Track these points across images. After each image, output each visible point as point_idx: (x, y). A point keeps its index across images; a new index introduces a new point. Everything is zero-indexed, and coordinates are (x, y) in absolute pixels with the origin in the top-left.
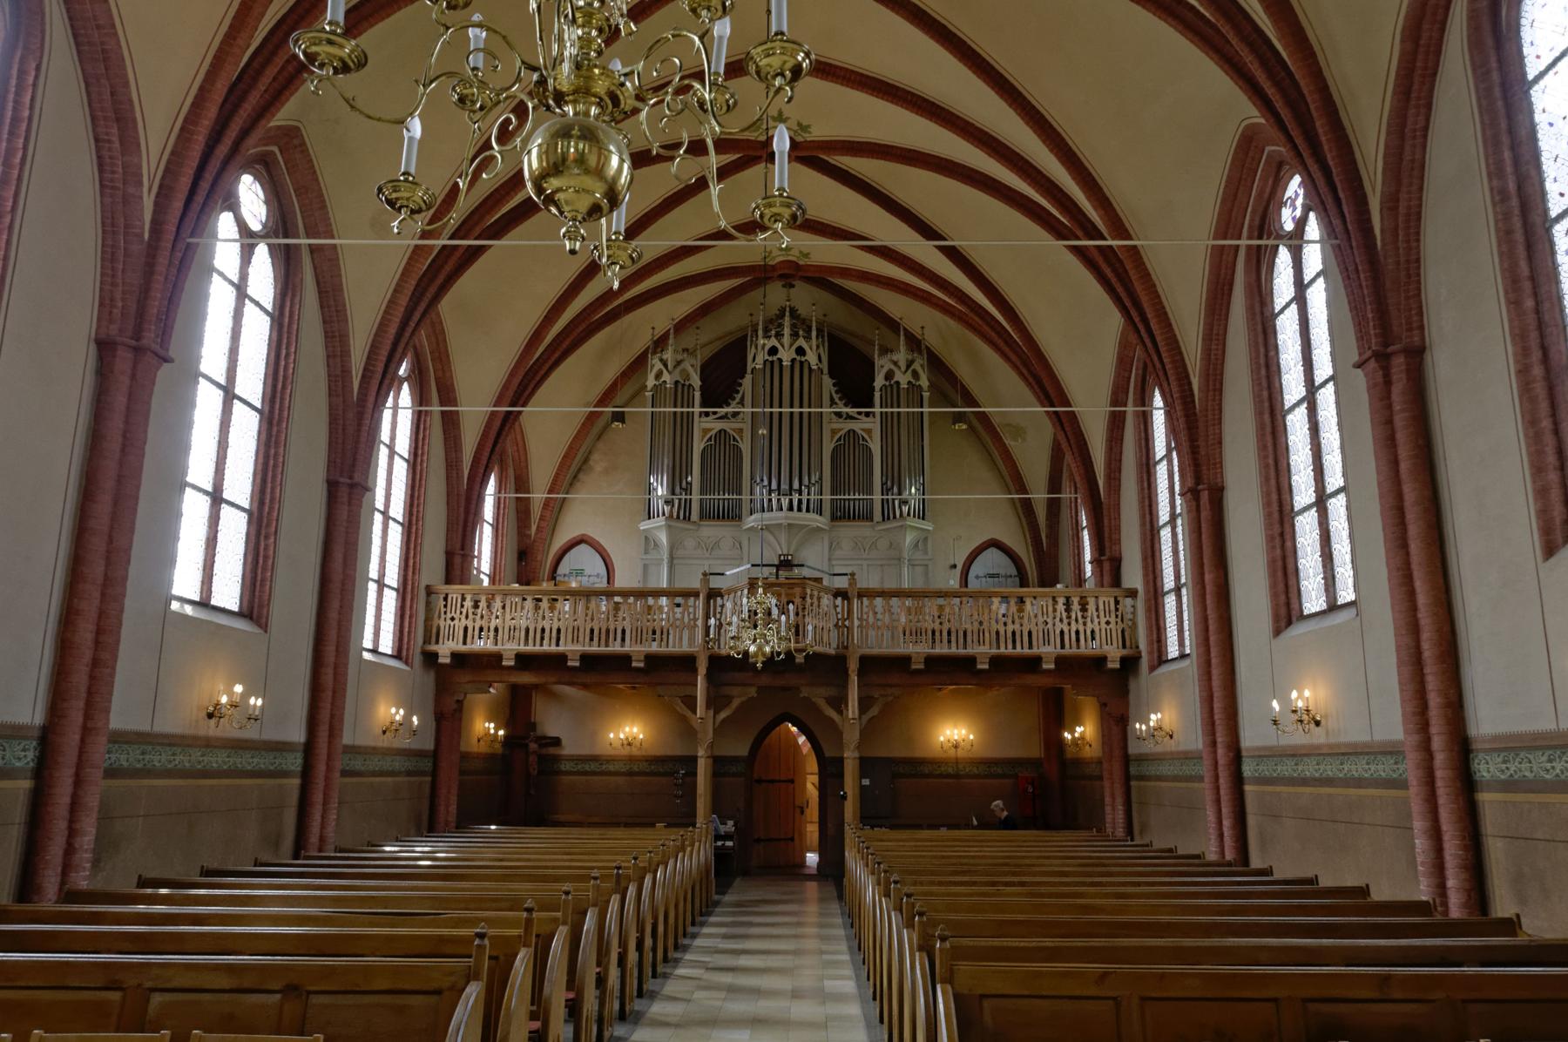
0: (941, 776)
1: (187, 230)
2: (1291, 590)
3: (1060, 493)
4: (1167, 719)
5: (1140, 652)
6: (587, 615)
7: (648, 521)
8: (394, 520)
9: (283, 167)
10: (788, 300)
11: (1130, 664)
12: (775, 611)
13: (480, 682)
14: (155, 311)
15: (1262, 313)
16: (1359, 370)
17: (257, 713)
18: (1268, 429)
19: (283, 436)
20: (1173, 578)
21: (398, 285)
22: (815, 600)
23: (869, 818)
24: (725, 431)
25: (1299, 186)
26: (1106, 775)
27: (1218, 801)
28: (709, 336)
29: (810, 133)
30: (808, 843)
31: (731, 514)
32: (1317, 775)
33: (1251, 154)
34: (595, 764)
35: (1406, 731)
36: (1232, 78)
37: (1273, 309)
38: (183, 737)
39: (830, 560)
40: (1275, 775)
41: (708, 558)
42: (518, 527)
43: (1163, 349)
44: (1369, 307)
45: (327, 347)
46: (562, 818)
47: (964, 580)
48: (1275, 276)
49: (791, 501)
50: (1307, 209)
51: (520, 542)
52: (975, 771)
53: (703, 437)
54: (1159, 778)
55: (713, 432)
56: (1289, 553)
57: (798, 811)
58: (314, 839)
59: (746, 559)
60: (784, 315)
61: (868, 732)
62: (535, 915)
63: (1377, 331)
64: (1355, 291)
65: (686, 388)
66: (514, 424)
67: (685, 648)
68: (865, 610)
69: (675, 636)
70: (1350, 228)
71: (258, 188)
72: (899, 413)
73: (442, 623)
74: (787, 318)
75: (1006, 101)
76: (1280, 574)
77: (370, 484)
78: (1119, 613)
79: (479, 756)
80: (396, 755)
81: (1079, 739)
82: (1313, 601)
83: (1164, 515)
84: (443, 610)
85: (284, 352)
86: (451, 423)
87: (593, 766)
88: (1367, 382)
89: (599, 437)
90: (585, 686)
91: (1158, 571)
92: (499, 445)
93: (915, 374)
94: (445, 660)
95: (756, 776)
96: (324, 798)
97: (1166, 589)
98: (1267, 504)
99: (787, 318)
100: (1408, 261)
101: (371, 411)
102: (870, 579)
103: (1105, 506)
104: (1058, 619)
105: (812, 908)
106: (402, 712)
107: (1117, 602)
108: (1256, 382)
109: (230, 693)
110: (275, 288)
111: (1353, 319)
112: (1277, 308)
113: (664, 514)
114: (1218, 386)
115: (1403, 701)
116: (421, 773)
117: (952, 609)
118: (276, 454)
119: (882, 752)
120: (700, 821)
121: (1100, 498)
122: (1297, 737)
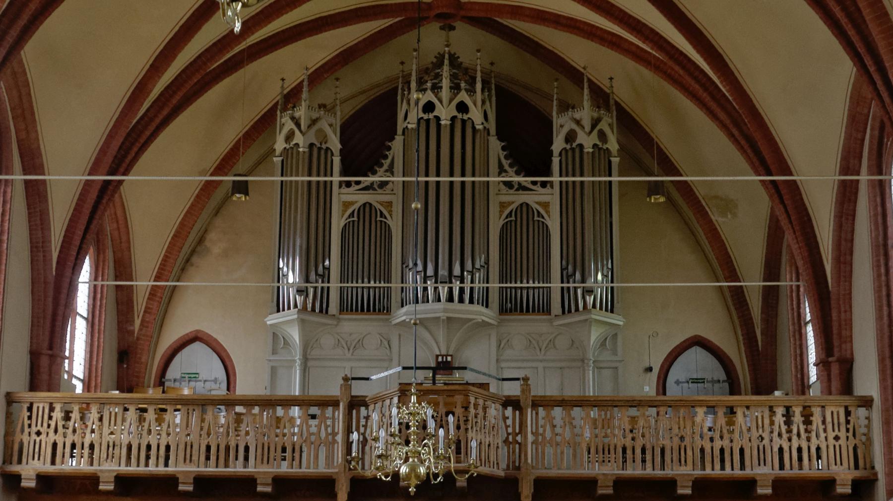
3: (778, 281)
5: (876, 474)
6: (202, 429)
10: (447, 46)
12: (431, 424)
22: (480, 411)
24: (370, 205)
39: (497, 360)
41: (350, 360)
42: (119, 322)
49: (451, 289)
51: (121, 340)
53: (344, 211)
55: (356, 207)
60: (442, 63)
65: (323, 152)
66: (113, 196)
67: (322, 469)
68: (541, 422)
69: (309, 455)
72: (582, 183)
73: (25, 438)
74: (446, 68)
78: (851, 427)
84: (27, 422)
89: (217, 212)
93: (602, 136)
94: (29, 483)
99: (446, 68)
103: (833, 297)
104: (776, 434)
107: (848, 413)
113: (296, 306)
121: (827, 286)
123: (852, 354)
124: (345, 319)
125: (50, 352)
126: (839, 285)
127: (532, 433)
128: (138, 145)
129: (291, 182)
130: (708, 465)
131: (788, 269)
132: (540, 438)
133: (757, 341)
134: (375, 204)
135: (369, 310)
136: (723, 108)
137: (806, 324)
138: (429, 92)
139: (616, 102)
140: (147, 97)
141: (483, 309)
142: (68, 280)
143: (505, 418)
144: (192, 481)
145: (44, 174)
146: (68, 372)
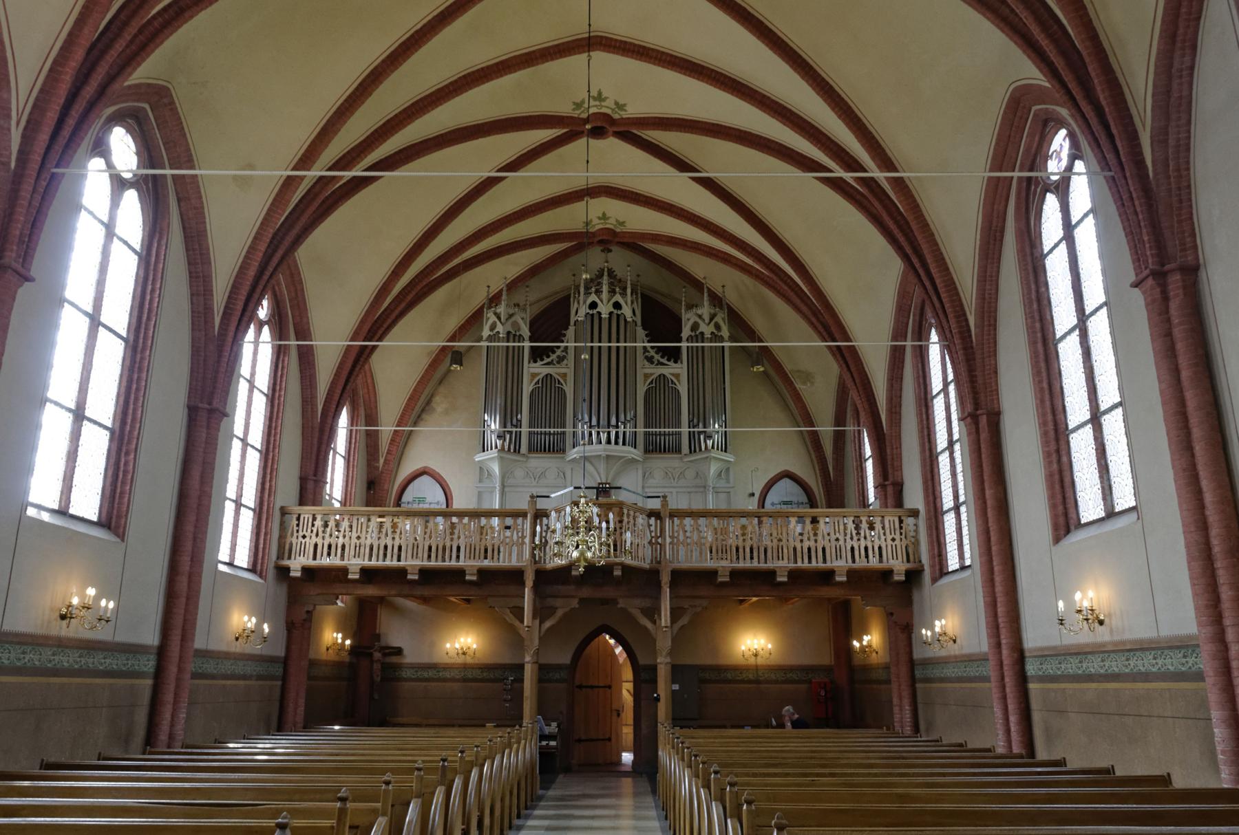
0: (742, 681)
1: (54, 156)
2: (1068, 501)
3: (845, 426)
4: (950, 625)
5: (923, 566)
6: (425, 533)
7: (482, 454)
8: (253, 447)
9: (154, 124)
10: (607, 262)
11: (914, 576)
12: (596, 520)
13: (327, 594)
14: (18, 233)
15: (1032, 254)
16: (1136, 289)
17: (108, 615)
18: (1042, 357)
19: (147, 362)
20: (952, 498)
21: (257, 233)
22: (631, 518)
23: (679, 720)
24: (551, 375)
25: (1064, 139)
26: (893, 678)
27: (1004, 698)
28: (538, 294)
29: (625, 111)
30: (624, 744)
31: (555, 447)
32: (1102, 671)
33: (1019, 114)
34: (435, 672)
35: (1200, 624)
36: (1007, 35)
37: (1042, 250)
38: (32, 636)
40: (1059, 673)
41: (535, 486)
42: (368, 460)
43: (942, 291)
44: (1144, 231)
45: (191, 286)
46: (401, 720)
47: (762, 503)
48: (1043, 221)
49: (609, 433)
50: (1073, 158)
51: (369, 473)
52: (773, 677)
53: (532, 380)
54: (942, 680)
55: (541, 377)
56: (1066, 467)
57: (615, 714)
58: (163, 737)
59: (569, 484)
60: (603, 275)
61: (680, 639)
62: (349, 805)
63: (1153, 252)
64: (1130, 218)
66: (363, 366)
67: (514, 562)
68: (676, 528)
69: (505, 552)
70: (1123, 160)
71: (129, 140)
72: (703, 347)
73: (294, 540)
74: (605, 277)
75: (799, 73)
76: (1057, 487)
77: (228, 410)
78: (903, 531)
79: (326, 663)
80: (247, 660)
81: (867, 647)
82: (1090, 506)
83: (941, 441)
85: (150, 287)
86: (306, 358)
87: (431, 674)
88: (1145, 299)
89: (441, 382)
90: (425, 600)
91: (937, 493)
92: (350, 384)
93: (718, 327)
95: (577, 683)
96: (175, 698)
97: (945, 508)
98: (1043, 424)
99: (605, 277)
100: (1179, 189)
101: (230, 344)
102: (679, 502)
103: (887, 437)
105: (627, 802)
106: (254, 620)
107: (901, 521)
108: (1029, 315)
109: (83, 595)
110: (144, 230)
111: (1128, 243)
112: (1046, 250)
113: (496, 447)
114: (992, 322)
115: (1195, 595)
116: (271, 678)
117: (753, 527)
118: (139, 379)
119: (689, 661)
120: (526, 721)
121: (883, 430)
122: (1082, 636)
123: (902, 479)
124: (532, 457)
125: (315, 478)
126: (891, 430)
127: (670, 537)
128: (383, 329)
129: (494, 346)
130: (799, 560)
131: (852, 421)
132: (675, 540)
133: (829, 475)
134: (554, 374)
135: (549, 451)
136: (806, 304)
137: (866, 460)
138: (593, 295)
139: (727, 304)
140: (390, 293)
141: (632, 449)
142: (329, 426)
143: (650, 526)
144: (417, 572)
145: (311, 341)
146: (329, 495)
